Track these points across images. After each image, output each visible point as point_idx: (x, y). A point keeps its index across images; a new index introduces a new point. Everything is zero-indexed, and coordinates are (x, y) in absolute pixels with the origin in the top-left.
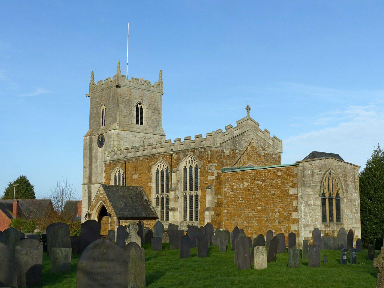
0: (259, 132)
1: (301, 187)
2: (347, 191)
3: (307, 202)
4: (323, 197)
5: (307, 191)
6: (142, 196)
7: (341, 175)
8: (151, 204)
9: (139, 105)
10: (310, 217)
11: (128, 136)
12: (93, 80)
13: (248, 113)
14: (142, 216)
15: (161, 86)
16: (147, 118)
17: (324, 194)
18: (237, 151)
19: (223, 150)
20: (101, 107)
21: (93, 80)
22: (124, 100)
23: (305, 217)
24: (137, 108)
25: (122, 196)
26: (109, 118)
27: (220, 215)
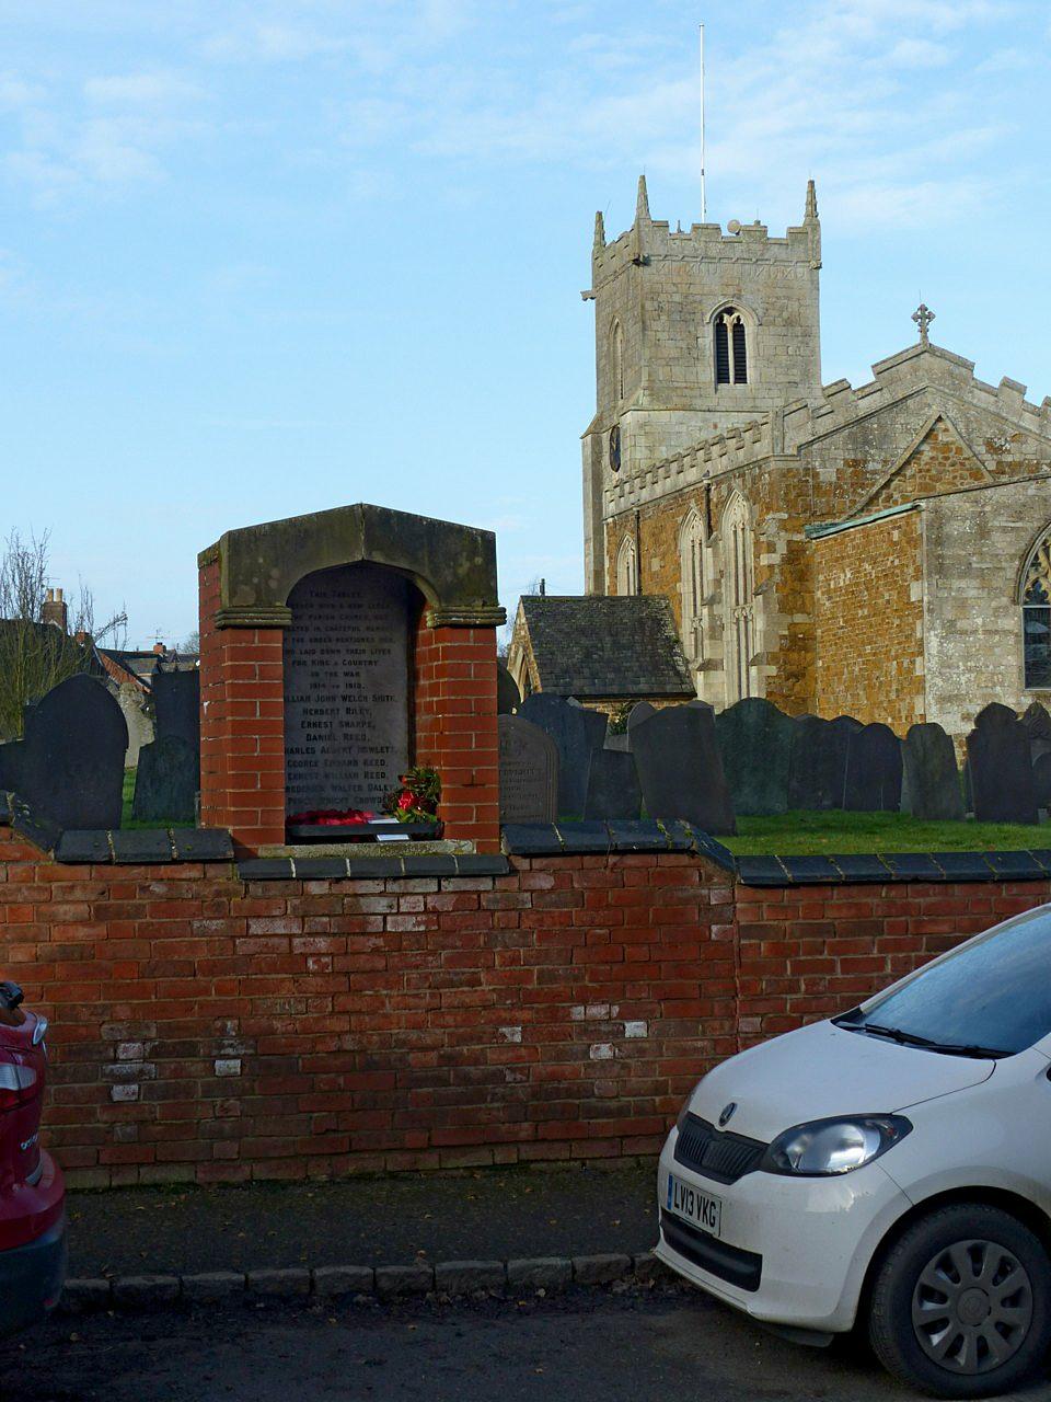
0: (971, 392)
1: (930, 574)
3: (952, 623)
4: (1031, 602)
5: (954, 587)
6: (658, 624)
8: (682, 650)
9: (726, 316)
11: (684, 429)
12: (601, 233)
13: (924, 331)
14: (633, 689)
15: (810, 237)
16: (757, 357)
18: (871, 466)
19: (810, 466)
20: (616, 332)
21: (601, 233)
22: (666, 307)
23: (943, 671)
24: (720, 329)
25: (582, 631)
26: (629, 370)
27: (804, 675)
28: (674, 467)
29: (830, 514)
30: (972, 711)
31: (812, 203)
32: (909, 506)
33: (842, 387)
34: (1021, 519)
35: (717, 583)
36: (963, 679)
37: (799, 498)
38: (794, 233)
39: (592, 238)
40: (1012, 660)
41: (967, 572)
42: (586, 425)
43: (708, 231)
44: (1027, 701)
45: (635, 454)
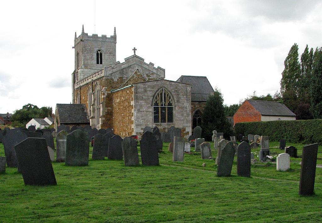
2: (178, 101)
3: (139, 109)
7: (173, 91)
10: (142, 119)
12: (76, 36)
13: (135, 52)
17: (156, 104)
21: (76, 36)
24: (98, 54)
28: (87, 79)
29: (116, 88)
30: (143, 128)
31: (115, 31)
32: (131, 85)
33: (119, 62)
34: (153, 89)
35: (94, 101)
36: (141, 121)
37: (110, 83)
38: (111, 37)
39: (74, 37)
40: (151, 117)
41: (142, 99)
42: (73, 72)
43: (95, 36)
44: (154, 126)
45: (80, 77)
